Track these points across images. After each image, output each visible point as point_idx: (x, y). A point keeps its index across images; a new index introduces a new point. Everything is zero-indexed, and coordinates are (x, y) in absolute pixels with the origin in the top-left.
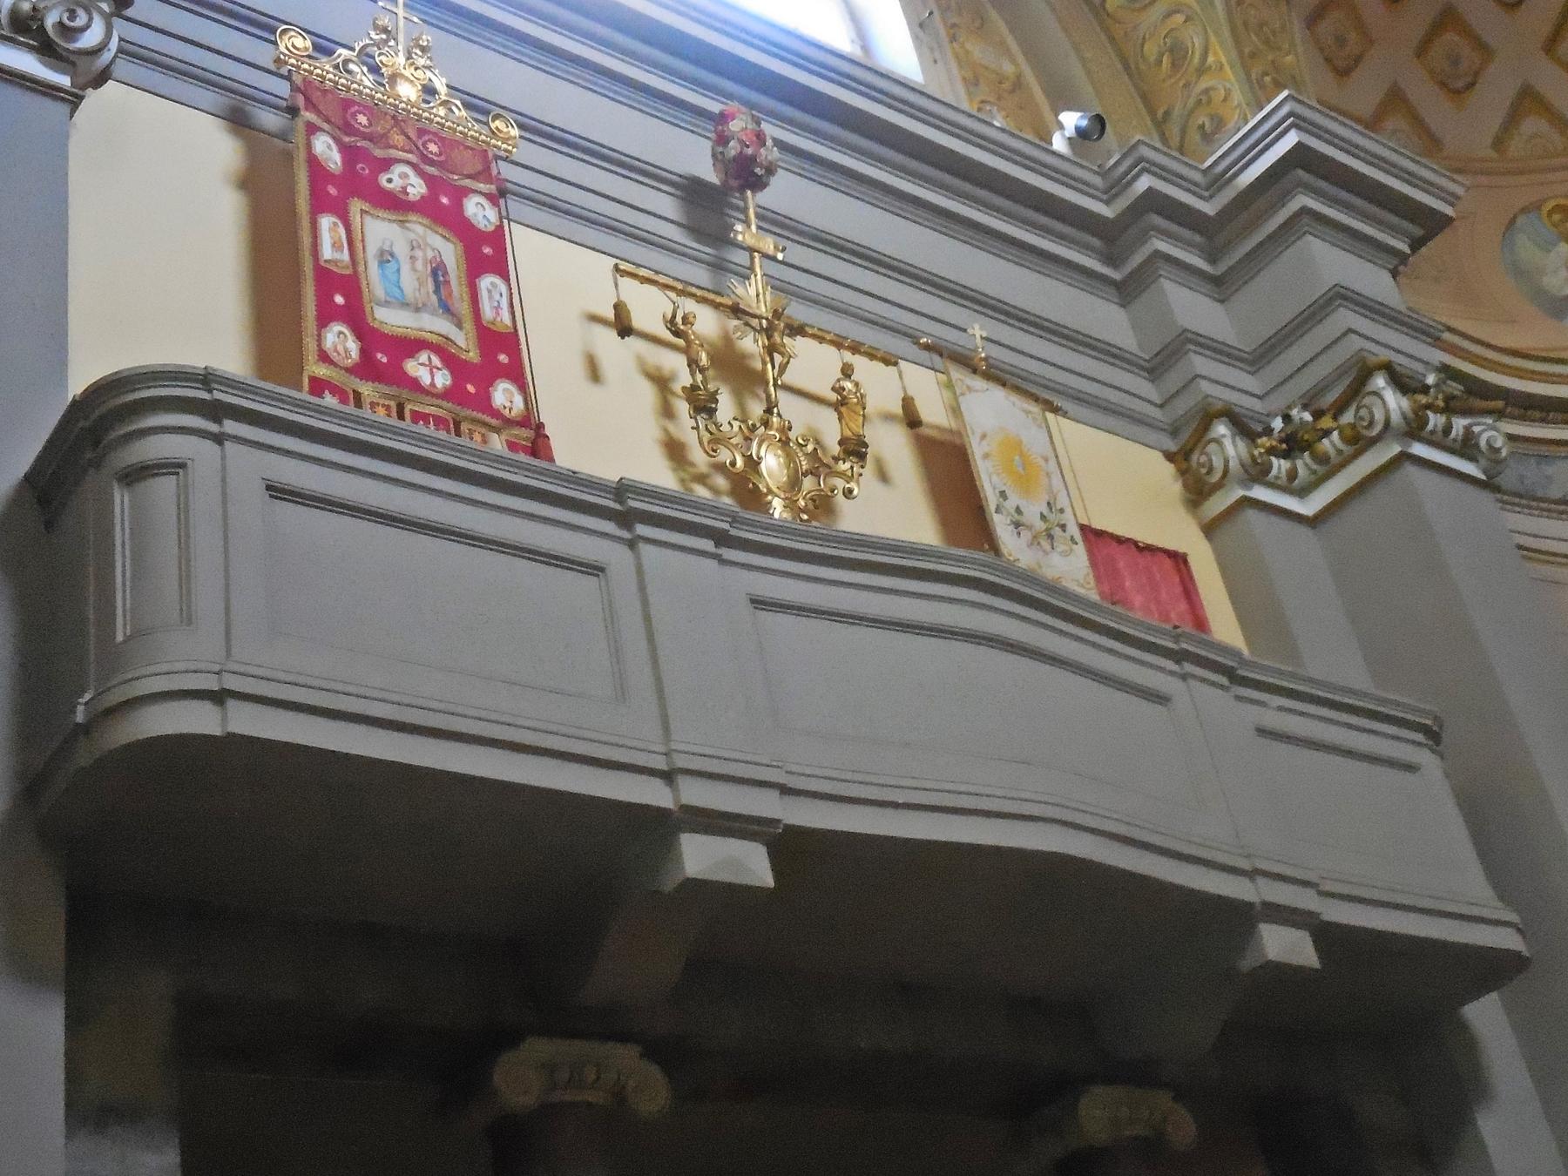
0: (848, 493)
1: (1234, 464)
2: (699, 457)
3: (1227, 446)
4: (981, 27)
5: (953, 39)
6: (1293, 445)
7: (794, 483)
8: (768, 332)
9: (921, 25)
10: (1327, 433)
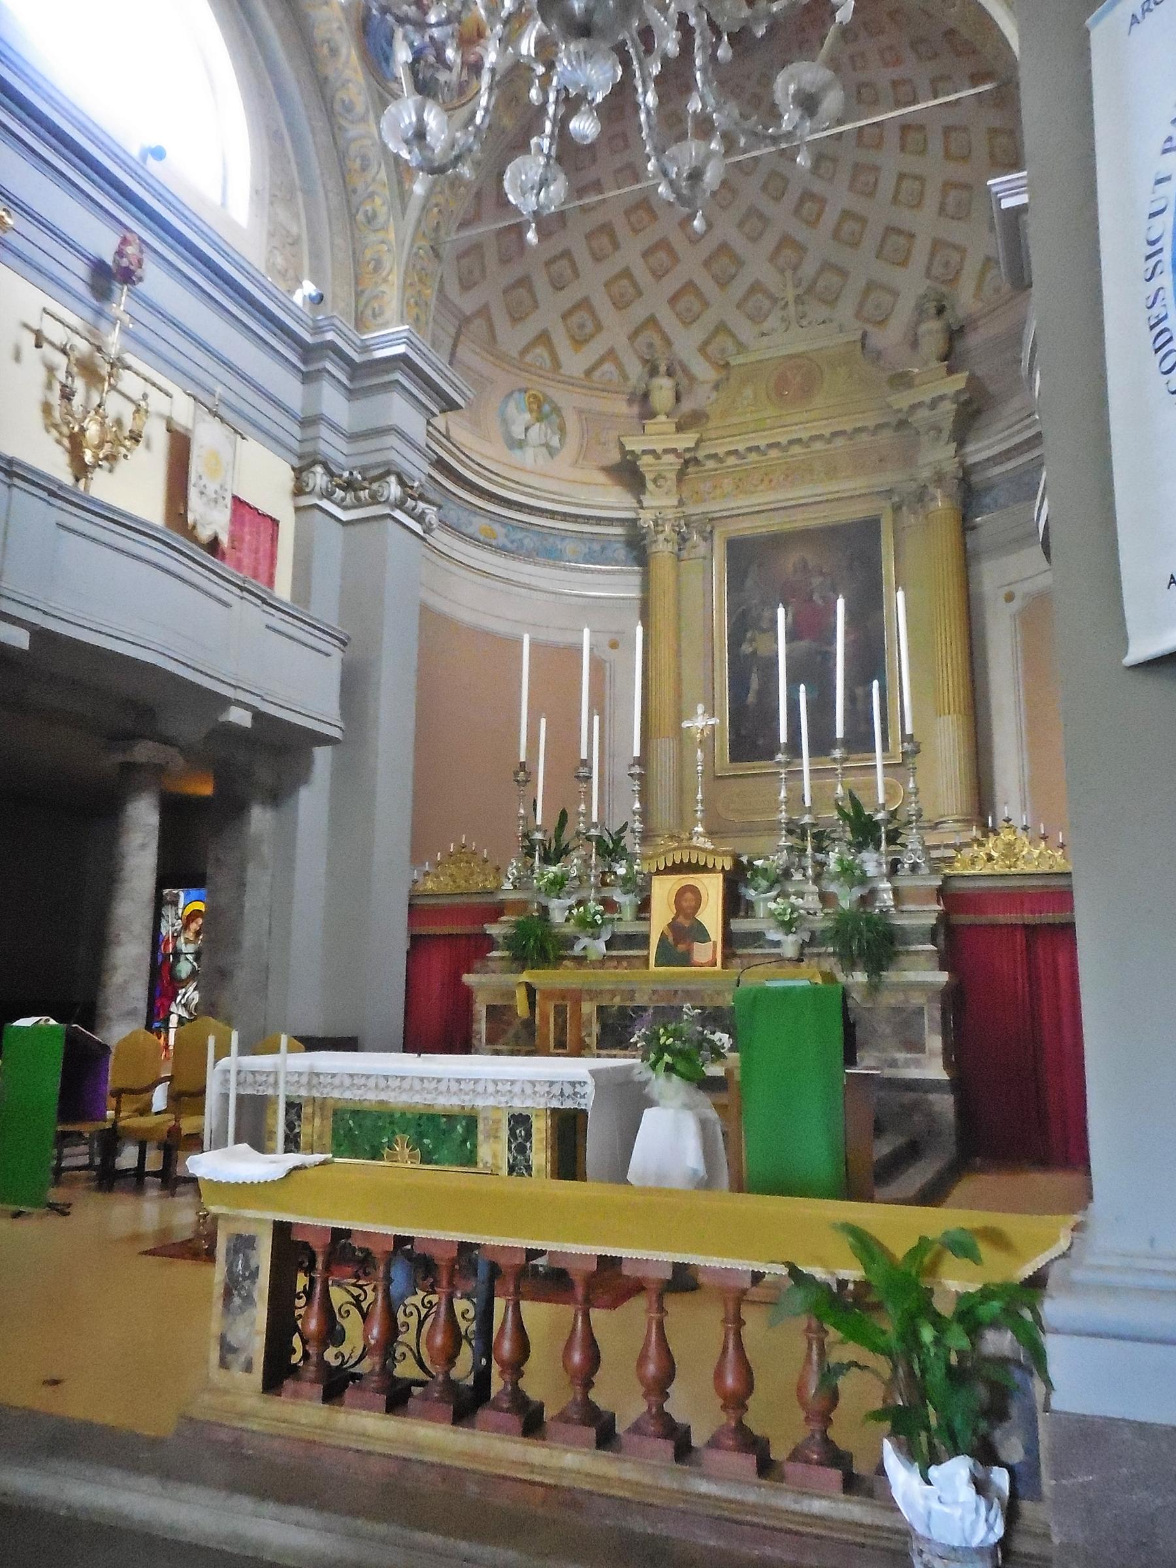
0: (125, 456)
1: (317, 489)
2: (57, 414)
3: (318, 478)
4: (290, 201)
5: (272, 203)
6: (349, 486)
7: (100, 446)
8: (112, 365)
9: (257, 192)
10: (365, 488)
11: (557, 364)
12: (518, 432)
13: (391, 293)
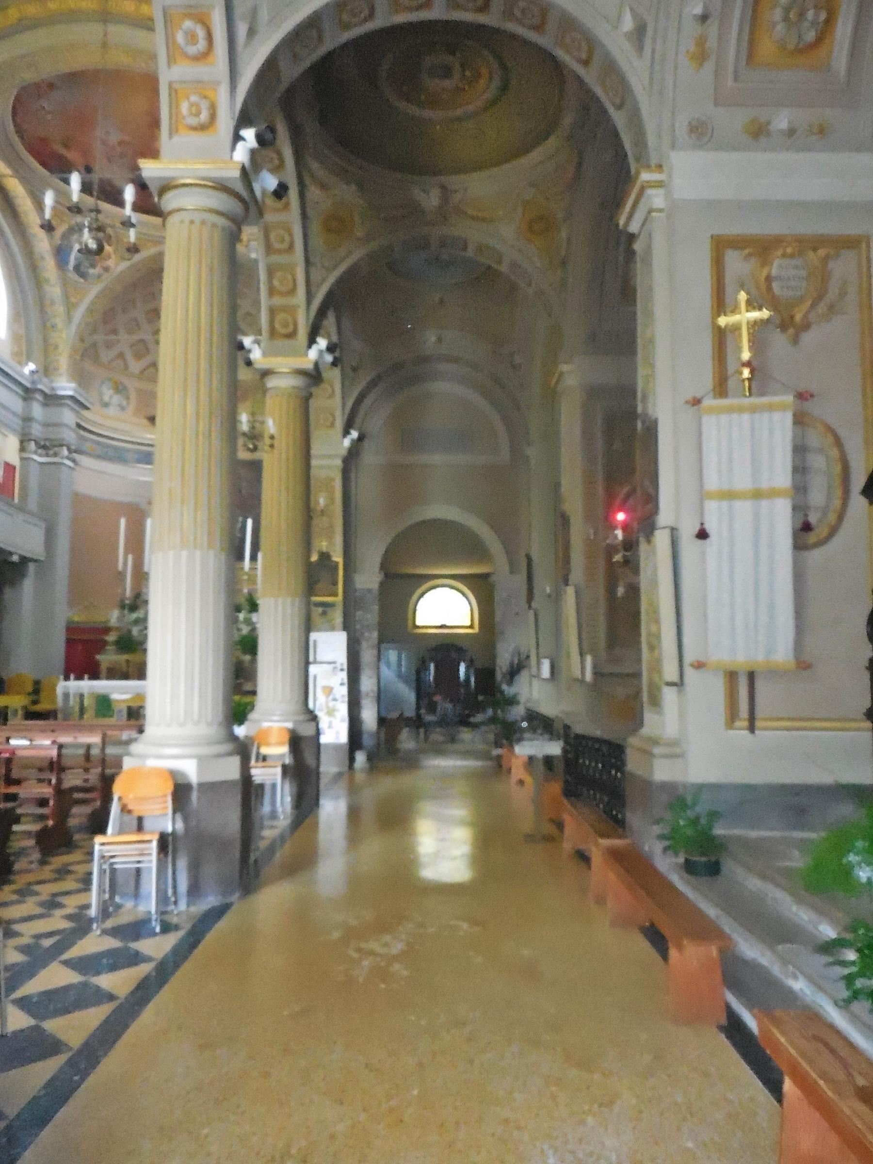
6: (44, 447)
11: (126, 367)
12: (106, 398)
13: (63, 361)
